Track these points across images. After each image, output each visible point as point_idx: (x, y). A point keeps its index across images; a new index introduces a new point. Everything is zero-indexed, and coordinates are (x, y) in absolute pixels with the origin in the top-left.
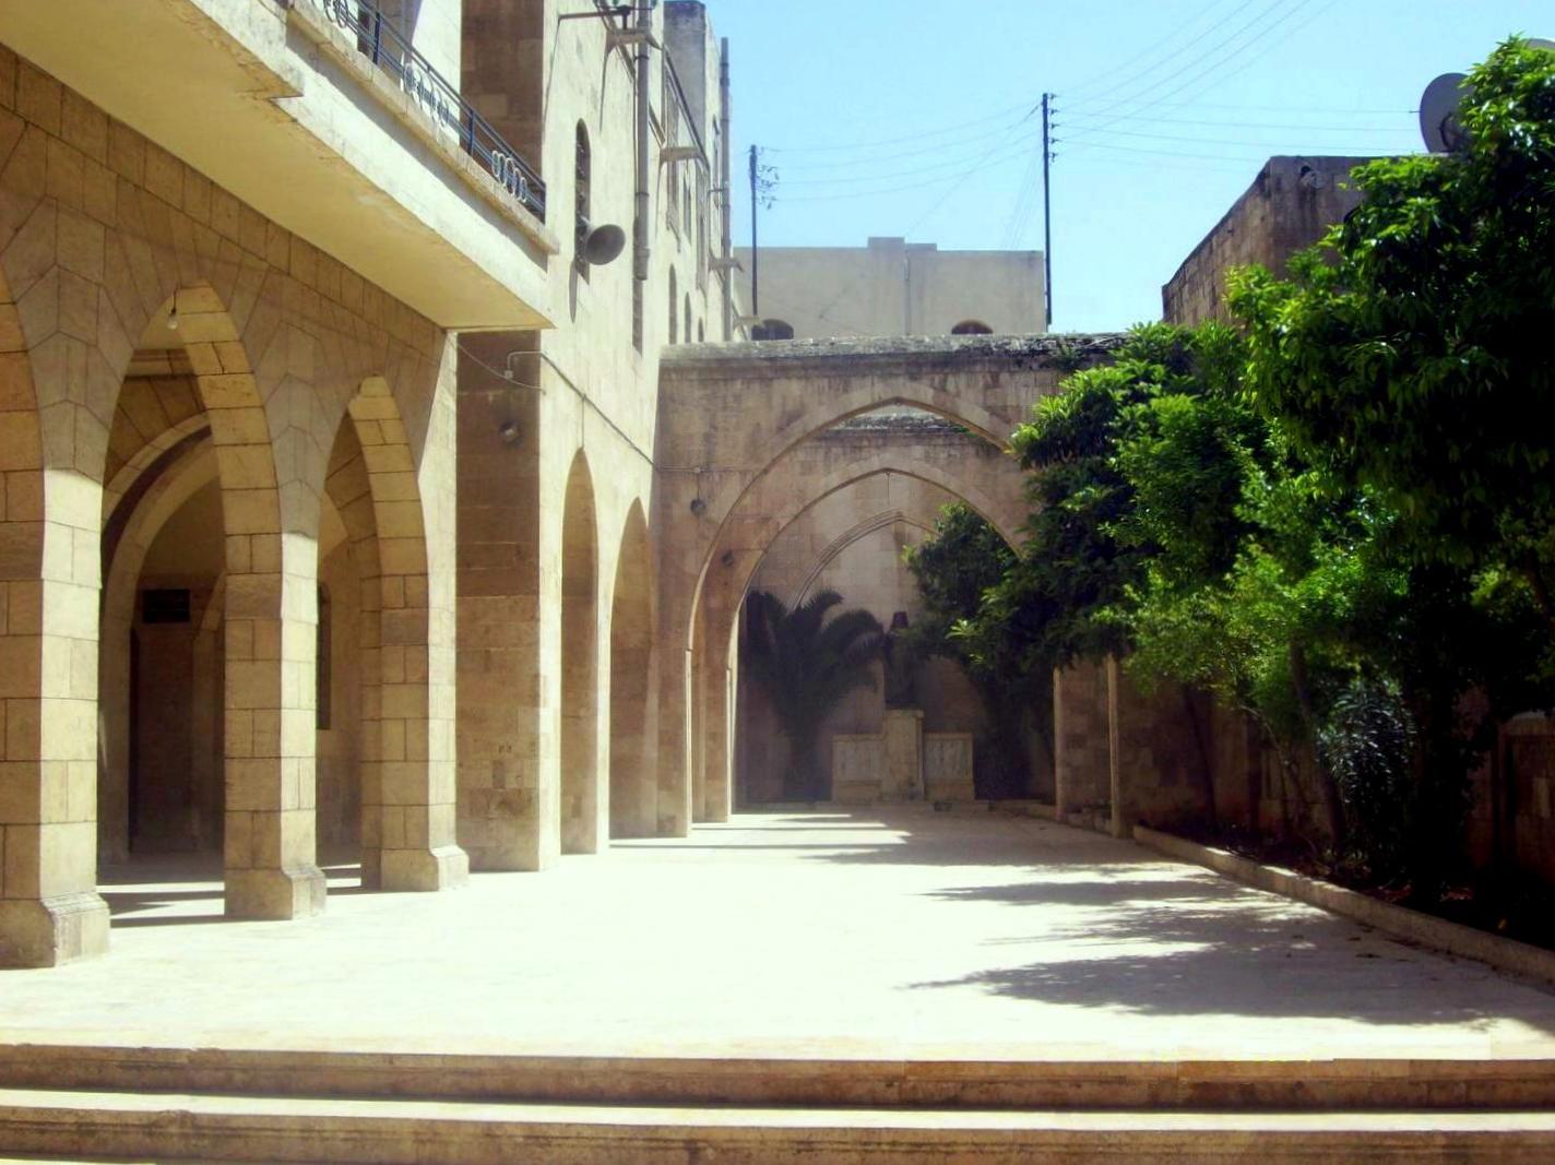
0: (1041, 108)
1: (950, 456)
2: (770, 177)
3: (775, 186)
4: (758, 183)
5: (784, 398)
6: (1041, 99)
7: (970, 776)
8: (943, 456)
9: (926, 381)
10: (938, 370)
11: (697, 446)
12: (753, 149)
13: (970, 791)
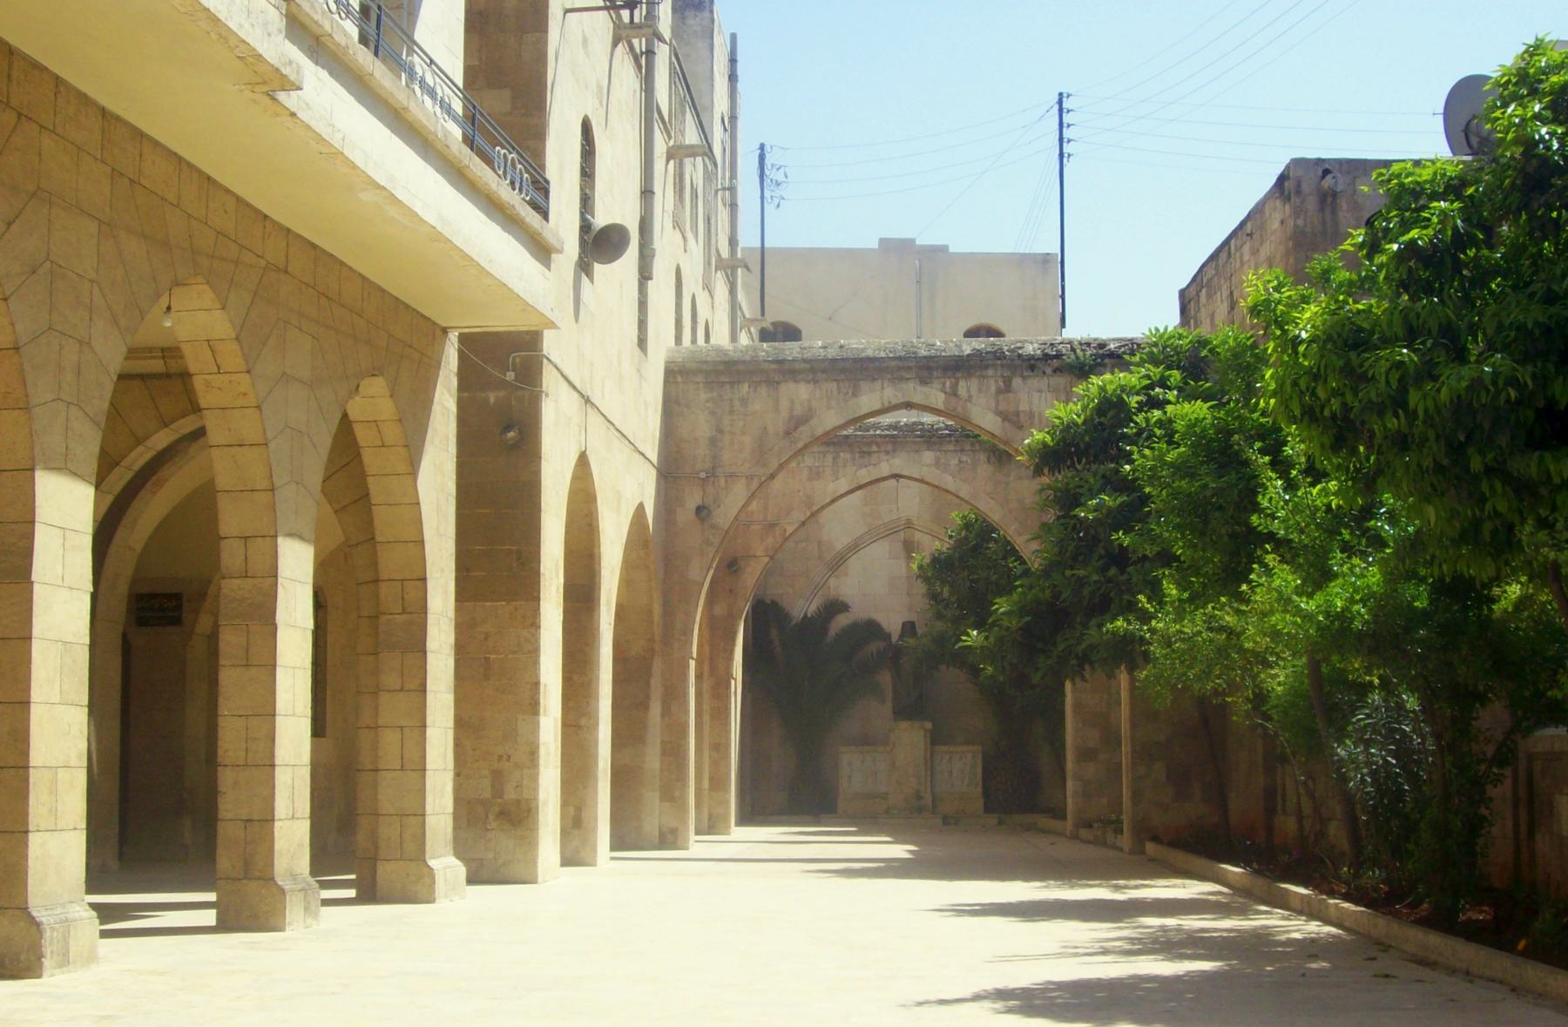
0: (1056, 107)
1: (960, 461)
2: (779, 176)
3: (784, 185)
4: (767, 182)
5: (792, 402)
6: (1056, 98)
7: (980, 790)
8: (954, 462)
9: (937, 385)
10: (950, 373)
11: (703, 451)
12: (762, 147)
13: (980, 804)
